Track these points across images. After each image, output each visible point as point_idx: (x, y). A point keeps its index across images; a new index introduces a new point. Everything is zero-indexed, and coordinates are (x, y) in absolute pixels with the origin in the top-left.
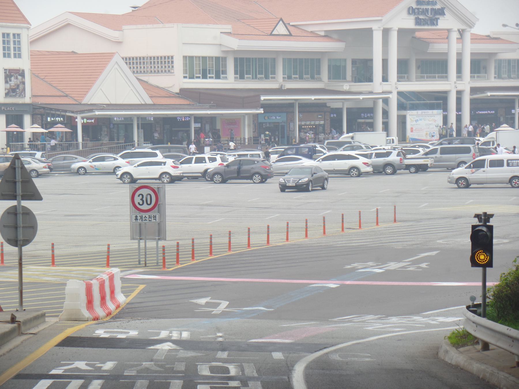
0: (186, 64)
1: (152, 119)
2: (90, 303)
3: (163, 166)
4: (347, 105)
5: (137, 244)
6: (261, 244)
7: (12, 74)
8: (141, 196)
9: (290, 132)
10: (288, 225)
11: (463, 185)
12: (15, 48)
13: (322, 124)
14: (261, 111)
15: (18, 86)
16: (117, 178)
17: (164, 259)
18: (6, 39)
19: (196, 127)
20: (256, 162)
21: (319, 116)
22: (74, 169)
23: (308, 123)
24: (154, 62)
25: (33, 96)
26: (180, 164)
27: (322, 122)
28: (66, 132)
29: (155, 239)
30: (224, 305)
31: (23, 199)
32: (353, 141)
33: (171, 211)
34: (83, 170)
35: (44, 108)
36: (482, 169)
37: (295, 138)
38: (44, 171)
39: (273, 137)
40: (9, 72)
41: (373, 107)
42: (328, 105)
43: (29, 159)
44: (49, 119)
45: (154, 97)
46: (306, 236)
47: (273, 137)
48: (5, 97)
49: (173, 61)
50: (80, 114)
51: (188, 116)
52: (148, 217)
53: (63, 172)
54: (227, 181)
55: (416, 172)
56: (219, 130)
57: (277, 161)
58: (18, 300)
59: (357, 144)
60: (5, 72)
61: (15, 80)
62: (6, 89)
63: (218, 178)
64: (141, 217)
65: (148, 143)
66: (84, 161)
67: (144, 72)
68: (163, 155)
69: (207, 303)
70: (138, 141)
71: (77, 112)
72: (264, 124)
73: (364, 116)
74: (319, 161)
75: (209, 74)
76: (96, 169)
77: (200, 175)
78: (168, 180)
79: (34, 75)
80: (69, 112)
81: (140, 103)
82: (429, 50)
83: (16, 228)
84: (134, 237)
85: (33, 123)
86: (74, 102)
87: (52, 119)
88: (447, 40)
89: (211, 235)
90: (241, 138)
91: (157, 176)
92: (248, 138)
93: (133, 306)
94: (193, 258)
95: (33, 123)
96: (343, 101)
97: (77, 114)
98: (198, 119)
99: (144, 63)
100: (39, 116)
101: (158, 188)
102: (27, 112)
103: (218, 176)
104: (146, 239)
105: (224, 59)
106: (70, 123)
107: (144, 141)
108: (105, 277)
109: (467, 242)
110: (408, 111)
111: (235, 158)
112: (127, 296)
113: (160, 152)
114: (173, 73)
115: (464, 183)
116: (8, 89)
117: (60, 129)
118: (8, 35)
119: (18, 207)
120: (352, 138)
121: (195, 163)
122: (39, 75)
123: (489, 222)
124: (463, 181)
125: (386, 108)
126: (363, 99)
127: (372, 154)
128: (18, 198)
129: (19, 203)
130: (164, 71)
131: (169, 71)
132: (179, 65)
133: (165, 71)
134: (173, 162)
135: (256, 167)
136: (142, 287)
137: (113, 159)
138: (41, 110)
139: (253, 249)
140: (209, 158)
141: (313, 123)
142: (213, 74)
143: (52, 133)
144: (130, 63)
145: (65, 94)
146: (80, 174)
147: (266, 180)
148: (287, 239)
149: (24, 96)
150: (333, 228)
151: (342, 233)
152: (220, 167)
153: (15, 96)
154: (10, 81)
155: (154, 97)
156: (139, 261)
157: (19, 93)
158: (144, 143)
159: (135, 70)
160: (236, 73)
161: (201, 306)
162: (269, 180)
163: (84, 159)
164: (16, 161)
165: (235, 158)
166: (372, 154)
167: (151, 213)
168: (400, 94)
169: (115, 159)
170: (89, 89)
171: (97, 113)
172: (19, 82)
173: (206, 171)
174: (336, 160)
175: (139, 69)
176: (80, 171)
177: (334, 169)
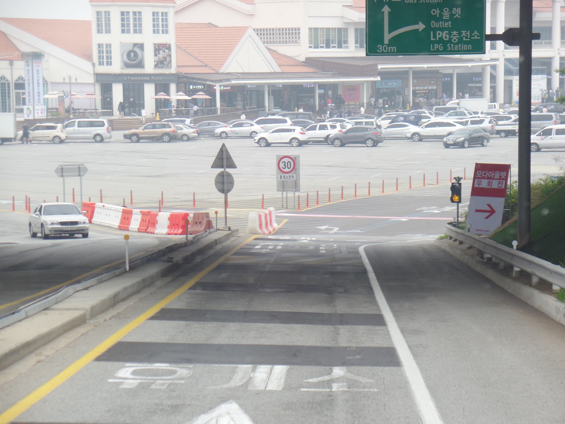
0: (311, 35)
1: (281, 86)
2: (261, 225)
3: (292, 133)
4: (457, 71)
5: (281, 195)
6: (364, 195)
7: (160, 48)
8: (284, 163)
9: (405, 97)
10: (383, 182)
11: (534, 149)
12: (163, 25)
13: (434, 89)
14: (378, 78)
15: (165, 58)
16: (255, 142)
17: (299, 204)
18: (155, 17)
19: (320, 93)
20: (369, 129)
21: (432, 82)
22: (217, 134)
23: (422, 88)
24: (283, 33)
25: (178, 66)
26: (306, 131)
27: (434, 87)
28: (206, 99)
29: (293, 191)
30: (336, 229)
31: (227, 168)
32: (459, 107)
33: (304, 172)
34: (225, 135)
35: (187, 77)
36: (550, 137)
37: (409, 102)
38: (193, 136)
39: (389, 102)
40: (158, 46)
41: (481, 72)
42: (440, 71)
43: (181, 126)
44: (191, 87)
45: (283, 65)
46: (397, 189)
47: (389, 102)
48: (154, 68)
49: (300, 32)
50: (219, 82)
51: (313, 83)
52: (288, 176)
53: (207, 136)
54: (345, 144)
55: (506, 136)
56: (341, 95)
57: (388, 127)
58: (224, 224)
59: (462, 110)
60: (154, 47)
61: (163, 53)
62: (155, 61)
63: (337, 142)
64: (284, 177)
65: (278, 109)
66: (226, 127)
67: (274, 42)
68: (291, 121)
69: (326, 228)
70: (269, 106)
71: (216, 81)
72: (381, 90)
73: (476, 80)
74: (422, 128)
75: (332, 43)
76: (236, 133)
77: (323, 139)
78: (297, 144)
79: (178, 47)
80: (209, 81)
81: (270, 71)
82: (536, 18)
83: (223, 183)
84: (279, 189)
85: (178, 91)
86: (213, 72)
87: (194, 87)
88: (551, 9)
89: (330, 189)
90: (360, 103)
91: (288, 141)
92: (367, 103)
93: (283, 230)
94: (317, 203)
95: (178, 91)
96: (454, 68)
97: (216, 83)
98: (322, 86)
99: (273, 34)
100: (183, 84)
101: (295, 157)
102: (173, 81)
103: (337, 141)
104: (287, 191)
105: (346, 30)
106: (210, 91)
107: (274, 107)
108: (267, 212)
109: (450, 193)
110: (515, 77)
111: (352, 126)
112: (278, 225)
113: (290, 119)
114: (299, 43)
115: (535, 148)
116: (157, 61)
117: (201, 96)
118: (157, 13)
119: (224, 172)
120: (458, 104)
121: (319, 129)
122: (181, 46)
123: (460, 181)
124: (535, 146)
125: (493, 73)
126: (472, 66)
127: (467, 122)
128: (224, 167)
129: (225, 170)
130: (291, 42)
131: (296, 41)
132: (305, 36)
133: (293, 42)
134: (301, 129)
135: (370, 134)
136: (286, 220)
137: (250, 125)
138: (184, 79)
139: (358, 198)
140: (330, 125)
141: (426, 88)
142: (335, 44)
143: (196, 99)
144: (261, 34)
145: (204, 64)
146: (222, 138)
147: (377, 144)
148: (383, 192)
149: (170, 67)
150: (417, 184)
151: (423, 188)
152: (340, 133)
153: (162, 67)
154: (159, 54)
155: (283, 65)
156: (283, 206)
157: (166, 64)
158: (274, 109)
159: (265, 40)
160: (356, 42)
161: (322, 230)
162: (380, 144)
163: (225, 125)
164: (224, 147)
165: (352, 126)
166: (467, 122)
167: (291, 174)
168: (507, 60)
169: (252, 125)
170: (226, 59)
171: (234, 82)
172: (166, 55)
173: (328, 136)
174: (437, 126)
175: (269, 40)
176: (222, 135)
177: (435, 135)
